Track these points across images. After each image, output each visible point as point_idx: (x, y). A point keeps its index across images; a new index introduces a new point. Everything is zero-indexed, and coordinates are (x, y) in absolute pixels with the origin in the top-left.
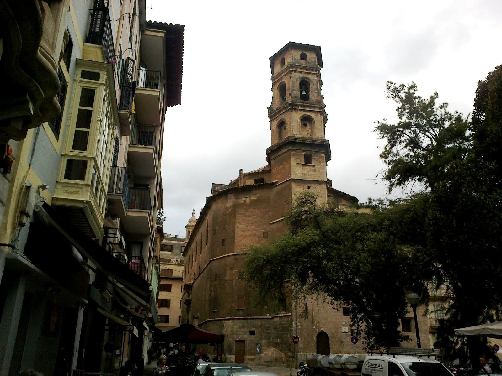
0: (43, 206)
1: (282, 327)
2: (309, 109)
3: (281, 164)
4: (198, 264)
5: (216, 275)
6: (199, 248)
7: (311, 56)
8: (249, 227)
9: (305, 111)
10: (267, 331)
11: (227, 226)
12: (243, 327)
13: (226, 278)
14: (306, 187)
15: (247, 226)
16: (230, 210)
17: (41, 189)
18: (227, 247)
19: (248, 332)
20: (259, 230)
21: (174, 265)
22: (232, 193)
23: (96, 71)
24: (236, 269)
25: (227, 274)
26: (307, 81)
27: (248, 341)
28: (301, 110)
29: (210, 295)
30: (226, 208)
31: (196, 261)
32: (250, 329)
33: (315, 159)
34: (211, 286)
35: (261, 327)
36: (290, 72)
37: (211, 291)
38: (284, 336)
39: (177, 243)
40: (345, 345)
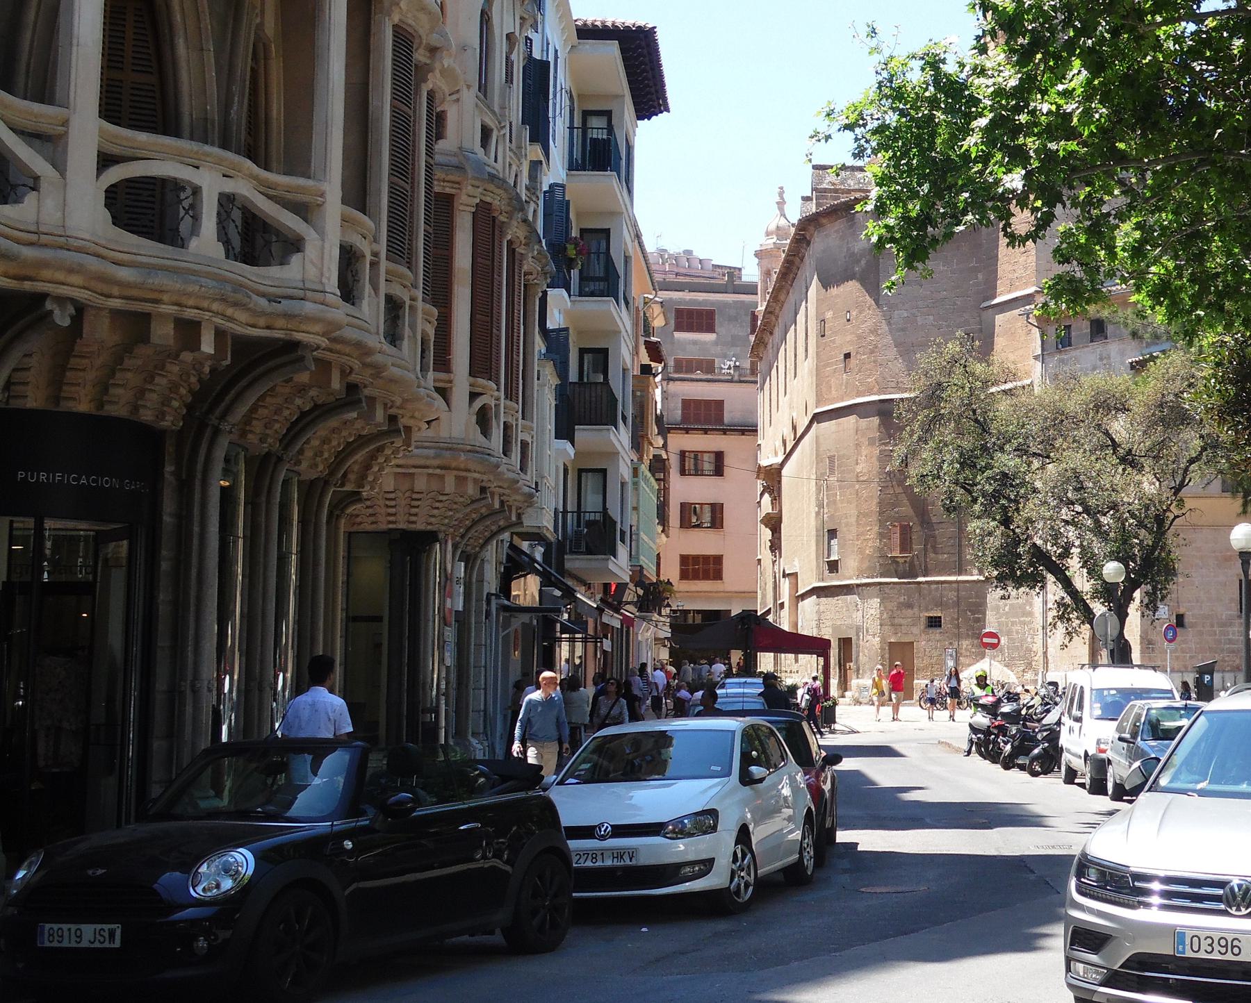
5: (831, 459)
12: (909, 606)
16: (863, 262)
19: (923, 621)
20: (948, 326)
21: (727, 381)
29: (818, 514)
30: (852, 255)
31: (806, 356)
32: (927, 610)
35: (958, 604)
38: (1014, 628)
39: (735, 302)
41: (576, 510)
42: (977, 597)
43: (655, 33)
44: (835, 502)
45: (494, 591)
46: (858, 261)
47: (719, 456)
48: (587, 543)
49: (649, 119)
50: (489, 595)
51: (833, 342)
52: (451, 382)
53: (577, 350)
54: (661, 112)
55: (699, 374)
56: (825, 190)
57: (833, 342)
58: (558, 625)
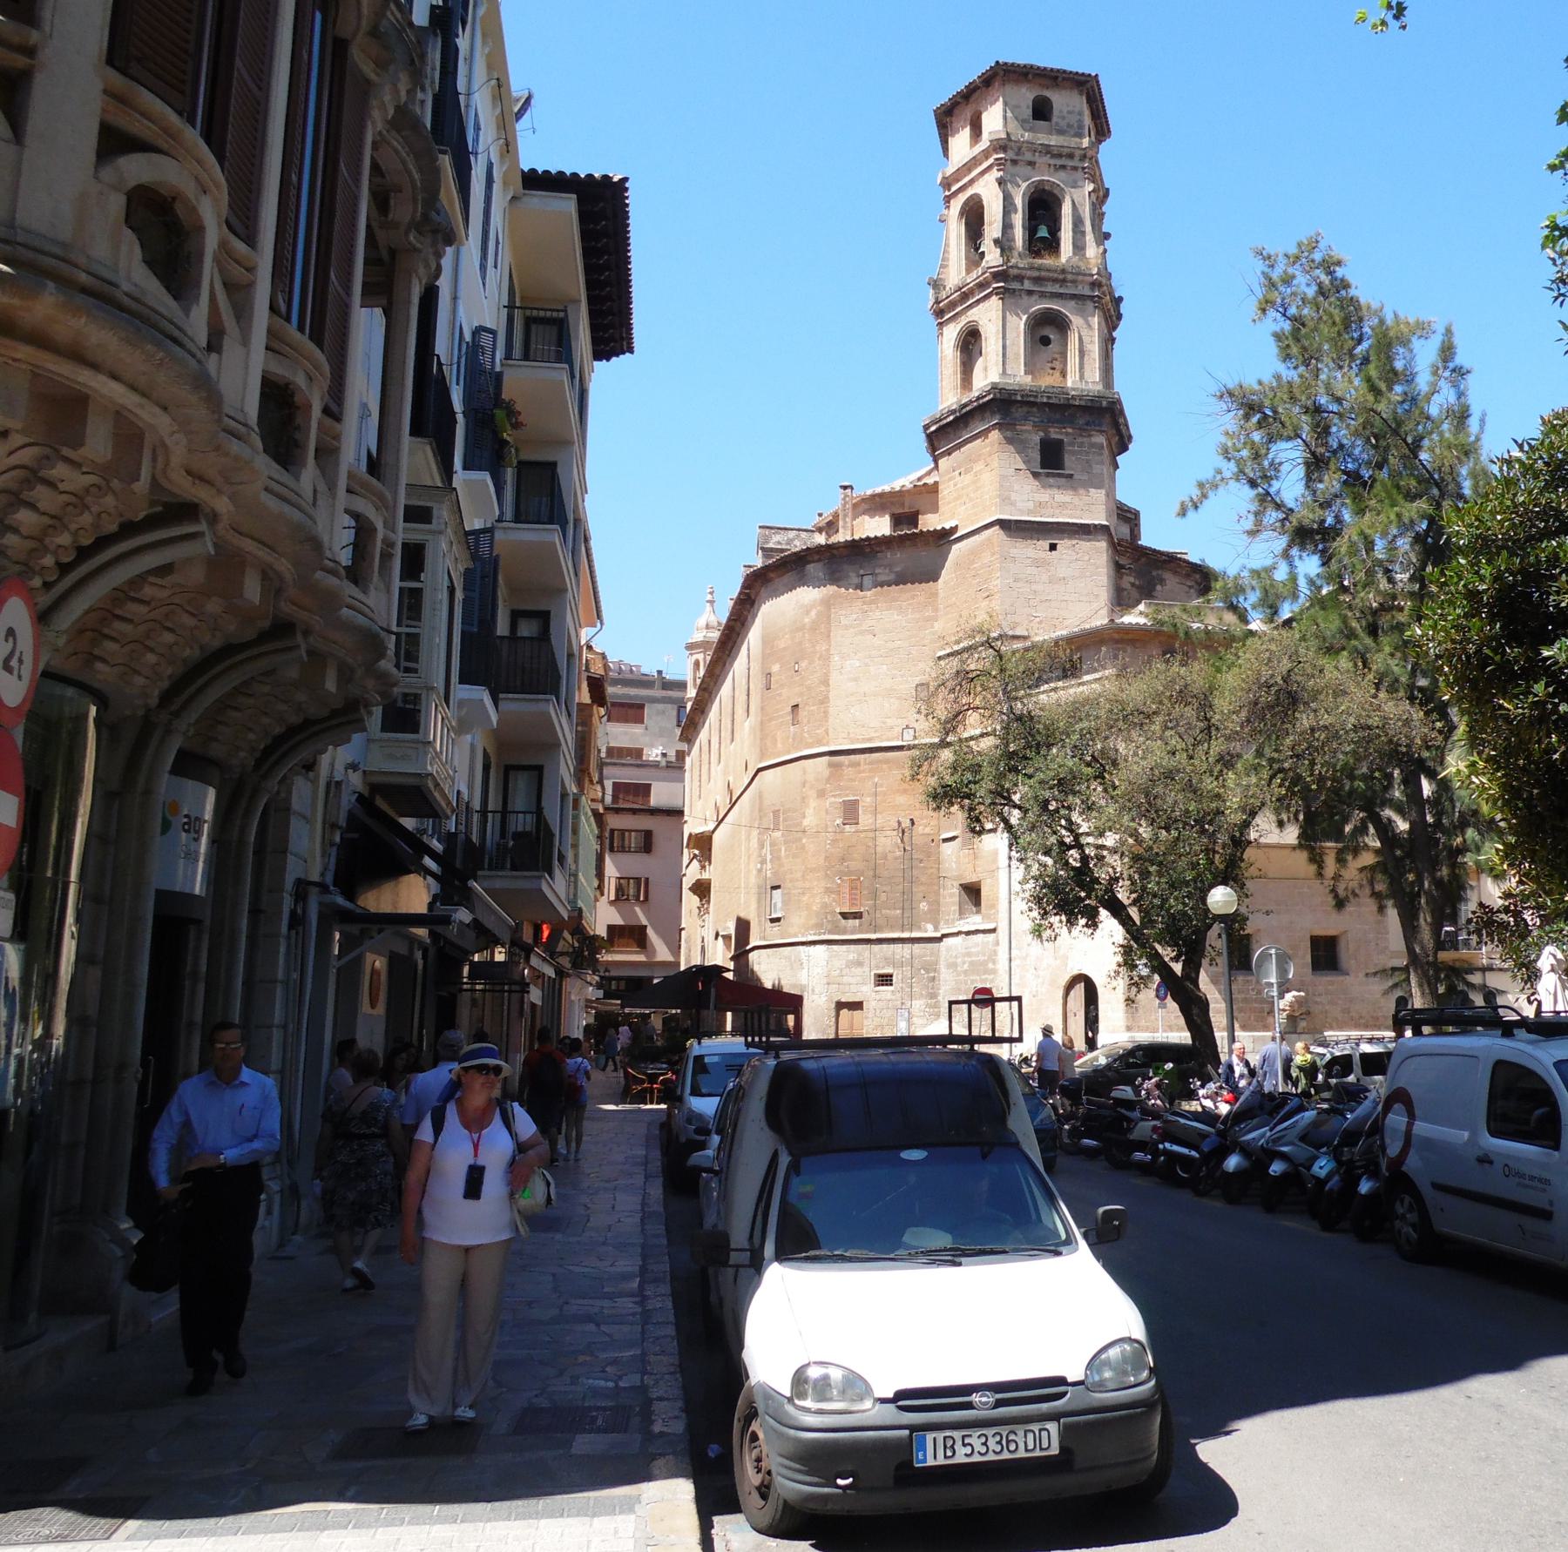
0: (357, 800)
1: (972, 963)
2: (1056, 289)
3: (967, 471)
4: (725, 773)
5: (776, 813)
6: (727, 722)
7: (1066, 103)
8: (872, 669)
9: (1043, 295)
10: (928, 972)
11: (804, 664)
12: (859, 964)
13: (806, 822)
14: (1046, 544)
15: (867, 665)
16: (813, 613)
17: (350, 771)
18: (806, 729)
22: (819, 560)
23: (421, 503)
24: (834, 796)
25: (809, 812)
26: (1051, 194)
27: (874, 1003)
28: (1030, 293)
29: (760, 871)
33: (1073, 453)
34: (762, 846)
36: (999, 165)
37: (763, 862)
40: (1140, 1011)
41: (500, 809)
42: (931, 955)
43: (627, 205)
44: (779, 858)
45: (315, 876)
46: (808, 612)
47: (648, 835)
48: (512, 859)
49: (608, 360)
50: (302, 887)
51: (780, 695)
52: (30, 51)
53: (508, 613)
54: (624, 353)
55: (629, 760)
56: (772, 550)
57: (780, 695)
58: (466, 970)
